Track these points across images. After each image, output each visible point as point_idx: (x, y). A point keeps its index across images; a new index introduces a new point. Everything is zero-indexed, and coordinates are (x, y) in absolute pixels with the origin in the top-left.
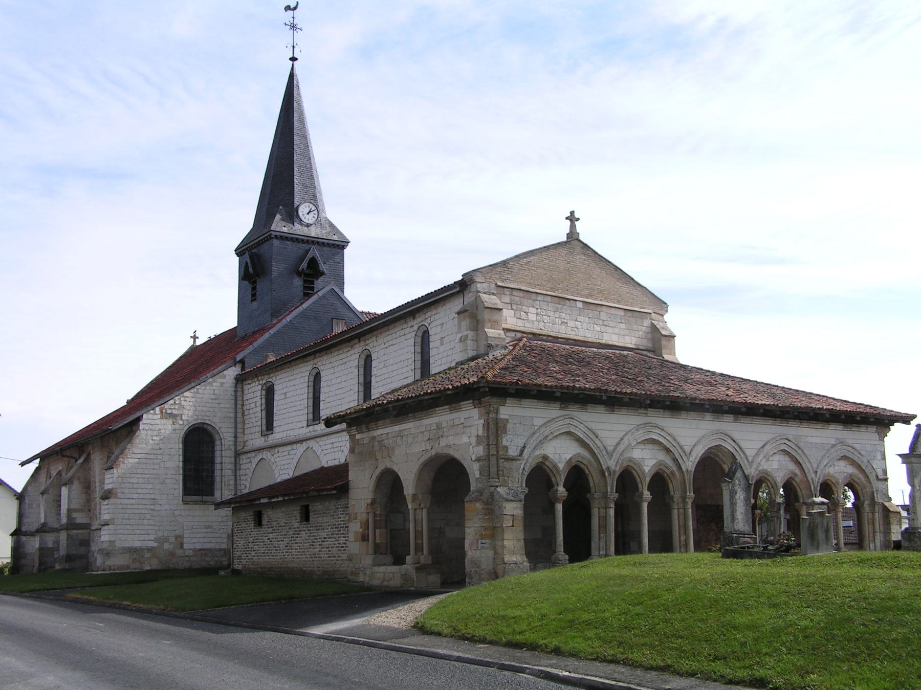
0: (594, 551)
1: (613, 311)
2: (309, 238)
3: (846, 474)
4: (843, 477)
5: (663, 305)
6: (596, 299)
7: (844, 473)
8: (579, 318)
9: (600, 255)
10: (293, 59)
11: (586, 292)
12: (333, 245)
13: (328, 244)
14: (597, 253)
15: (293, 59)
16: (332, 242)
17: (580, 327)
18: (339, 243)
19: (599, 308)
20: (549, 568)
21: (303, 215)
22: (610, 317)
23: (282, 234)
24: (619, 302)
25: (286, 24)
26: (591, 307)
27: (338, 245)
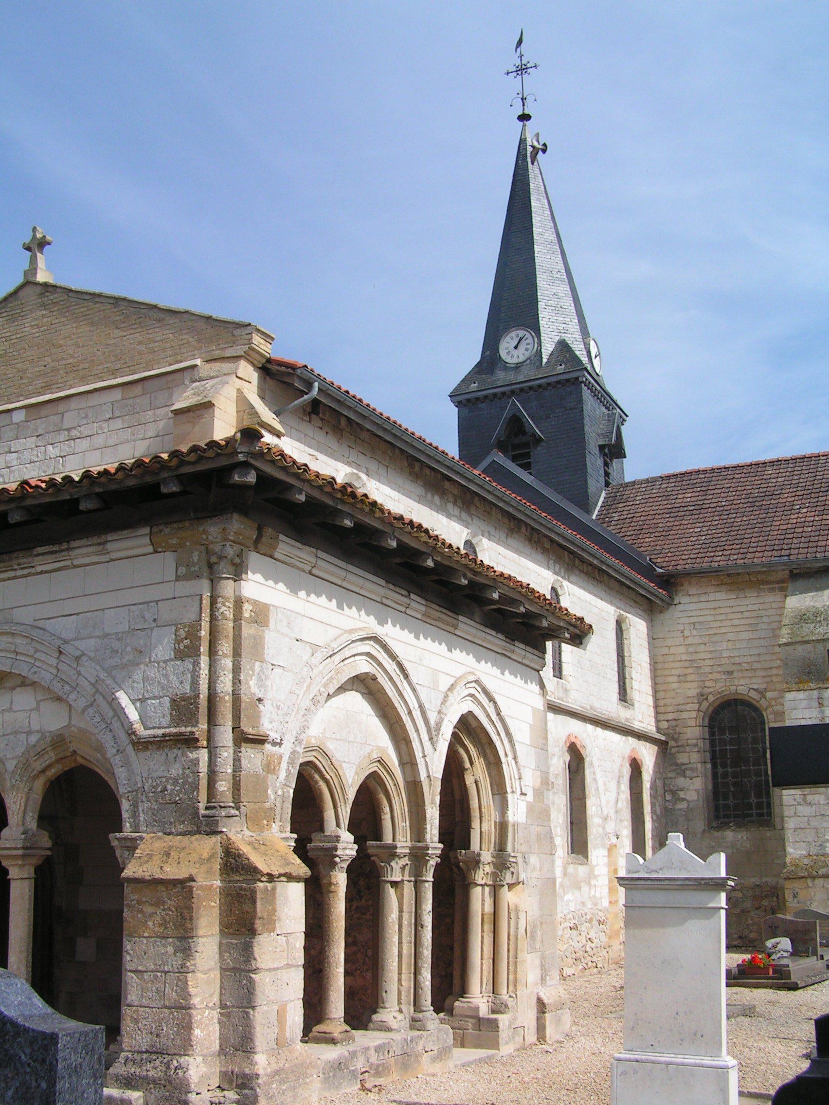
0: (728, 988)
1: (95, 399)
2: (513, 387)
3: (33, 739)
4: (20, 751)
5: (237, 332)
6: (60, 389)
7: (29, 733)
8: (15, 445)
9: (77, 292)
10: (524, 118)
11: (39, 383)
12: (558, 382)
13: (549, 384)
14: (71, 291)
15: (524, 118)
16: (554, 379)
17: (15, 463)
18: (567, 377)
19: (62, 407)
20: (253, 1008)
21: (508, 353)
22: (86, 417)
23: (468, 396)
24: (114, 373)
25: (535, 66)
26: (44, 411)
27: (567, 380)
